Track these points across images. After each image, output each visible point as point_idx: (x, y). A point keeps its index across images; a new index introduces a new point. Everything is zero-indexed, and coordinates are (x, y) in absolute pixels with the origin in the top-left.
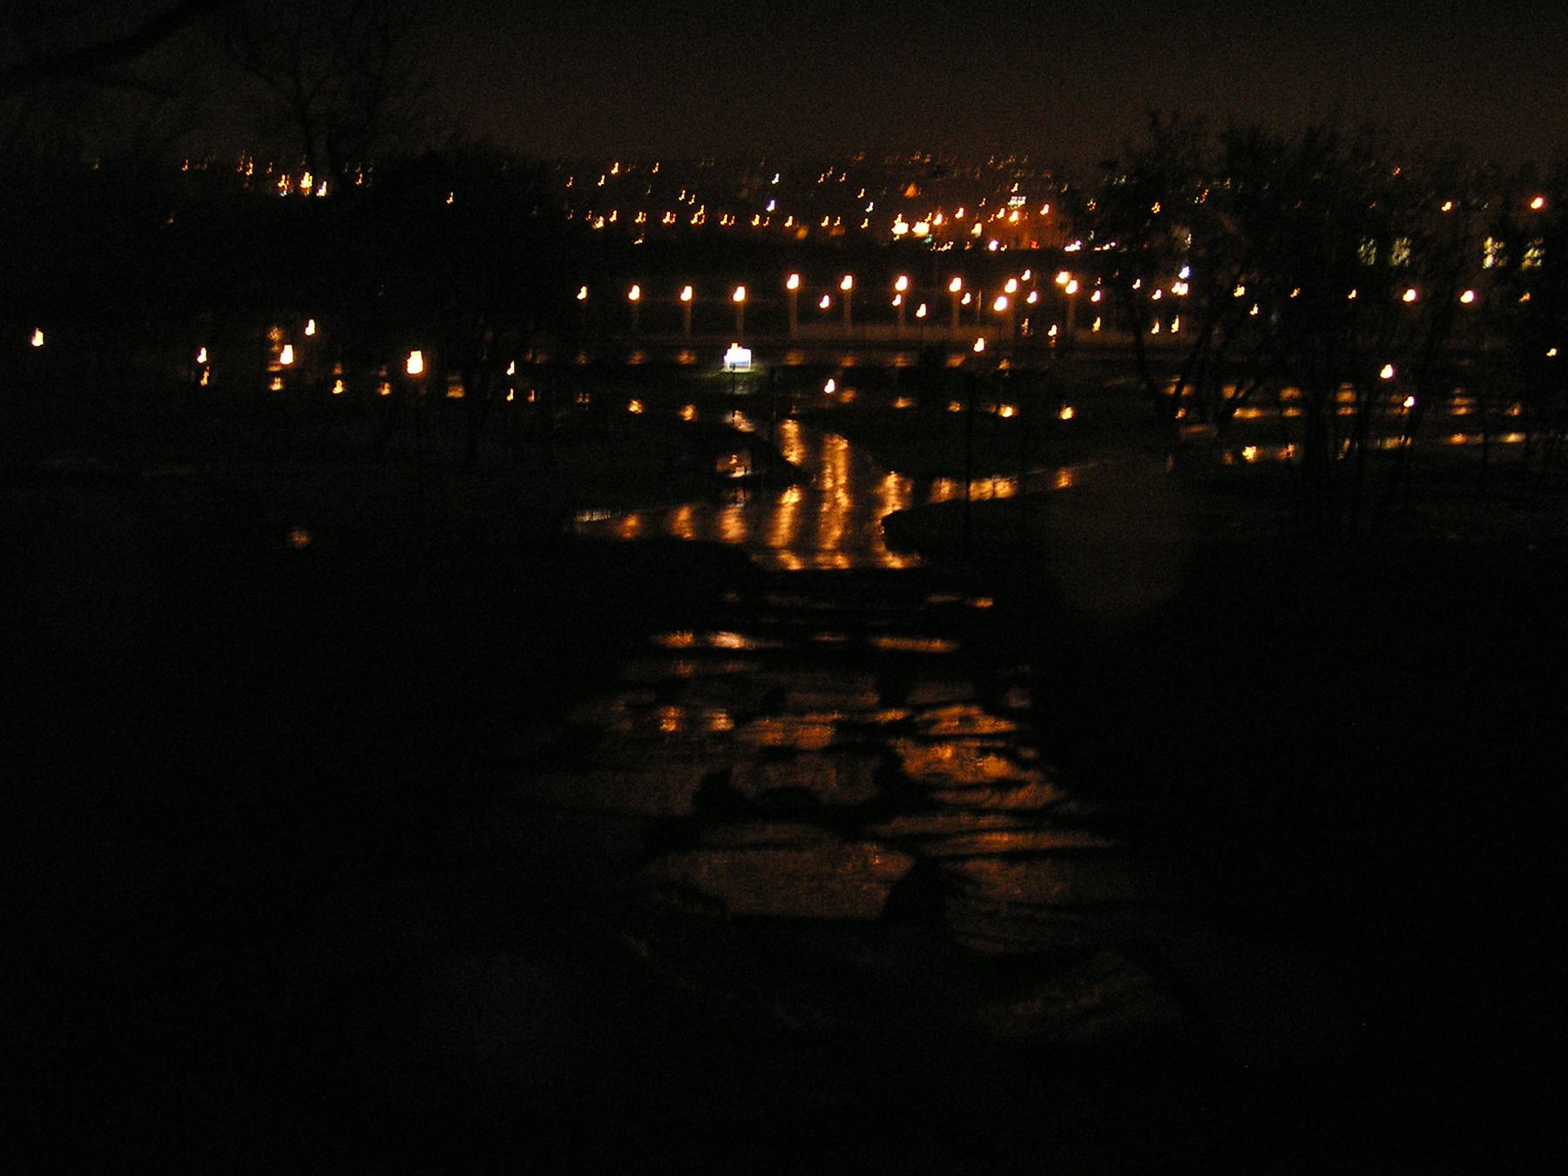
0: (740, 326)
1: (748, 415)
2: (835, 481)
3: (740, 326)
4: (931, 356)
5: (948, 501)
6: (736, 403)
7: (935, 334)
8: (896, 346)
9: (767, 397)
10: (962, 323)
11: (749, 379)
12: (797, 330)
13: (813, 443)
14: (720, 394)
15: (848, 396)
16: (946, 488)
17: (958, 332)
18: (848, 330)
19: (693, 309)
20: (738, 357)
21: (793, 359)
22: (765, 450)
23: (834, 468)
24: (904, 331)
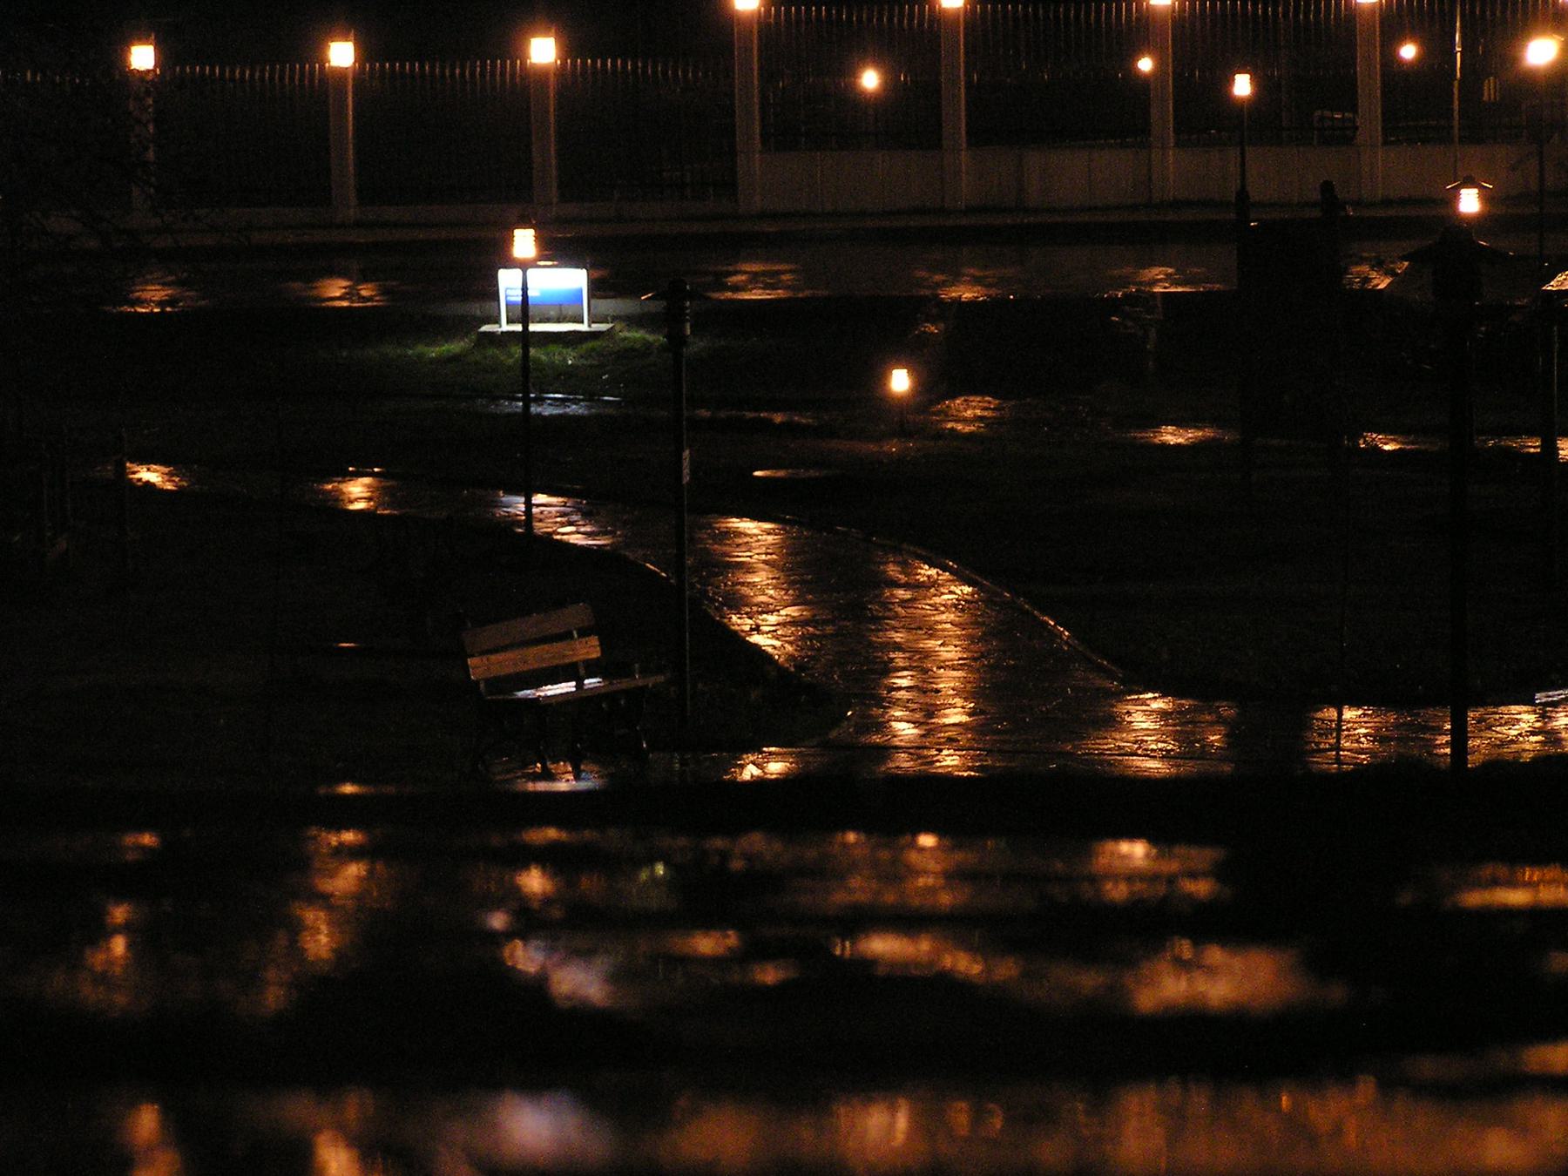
0: (546, 154)
1: (591, 502)
2: (927, 713)
3: (546, 154)
4: (1289, 256)
5: (498, 908)
6: (541, 457)
7: (1280, 178)
8: (1149, 231)
9: (662, 435)
10: (980, 136)
11: (592, 363)
12: (765, 180)
13: (841, 588)
14: (481, 422)
15: (969, 413)
16: (1356, 727)
17: (1381, 169)
18: (965, 173)
19: (560, 93)
20: (540, 282)
21: (752, 286)
22: (666, 611)
23: (922, 663)
24: (1174, 168)
